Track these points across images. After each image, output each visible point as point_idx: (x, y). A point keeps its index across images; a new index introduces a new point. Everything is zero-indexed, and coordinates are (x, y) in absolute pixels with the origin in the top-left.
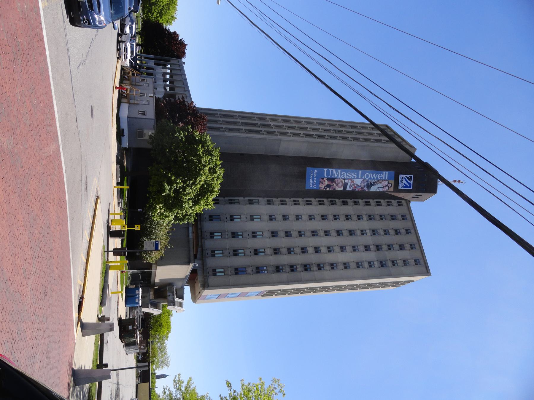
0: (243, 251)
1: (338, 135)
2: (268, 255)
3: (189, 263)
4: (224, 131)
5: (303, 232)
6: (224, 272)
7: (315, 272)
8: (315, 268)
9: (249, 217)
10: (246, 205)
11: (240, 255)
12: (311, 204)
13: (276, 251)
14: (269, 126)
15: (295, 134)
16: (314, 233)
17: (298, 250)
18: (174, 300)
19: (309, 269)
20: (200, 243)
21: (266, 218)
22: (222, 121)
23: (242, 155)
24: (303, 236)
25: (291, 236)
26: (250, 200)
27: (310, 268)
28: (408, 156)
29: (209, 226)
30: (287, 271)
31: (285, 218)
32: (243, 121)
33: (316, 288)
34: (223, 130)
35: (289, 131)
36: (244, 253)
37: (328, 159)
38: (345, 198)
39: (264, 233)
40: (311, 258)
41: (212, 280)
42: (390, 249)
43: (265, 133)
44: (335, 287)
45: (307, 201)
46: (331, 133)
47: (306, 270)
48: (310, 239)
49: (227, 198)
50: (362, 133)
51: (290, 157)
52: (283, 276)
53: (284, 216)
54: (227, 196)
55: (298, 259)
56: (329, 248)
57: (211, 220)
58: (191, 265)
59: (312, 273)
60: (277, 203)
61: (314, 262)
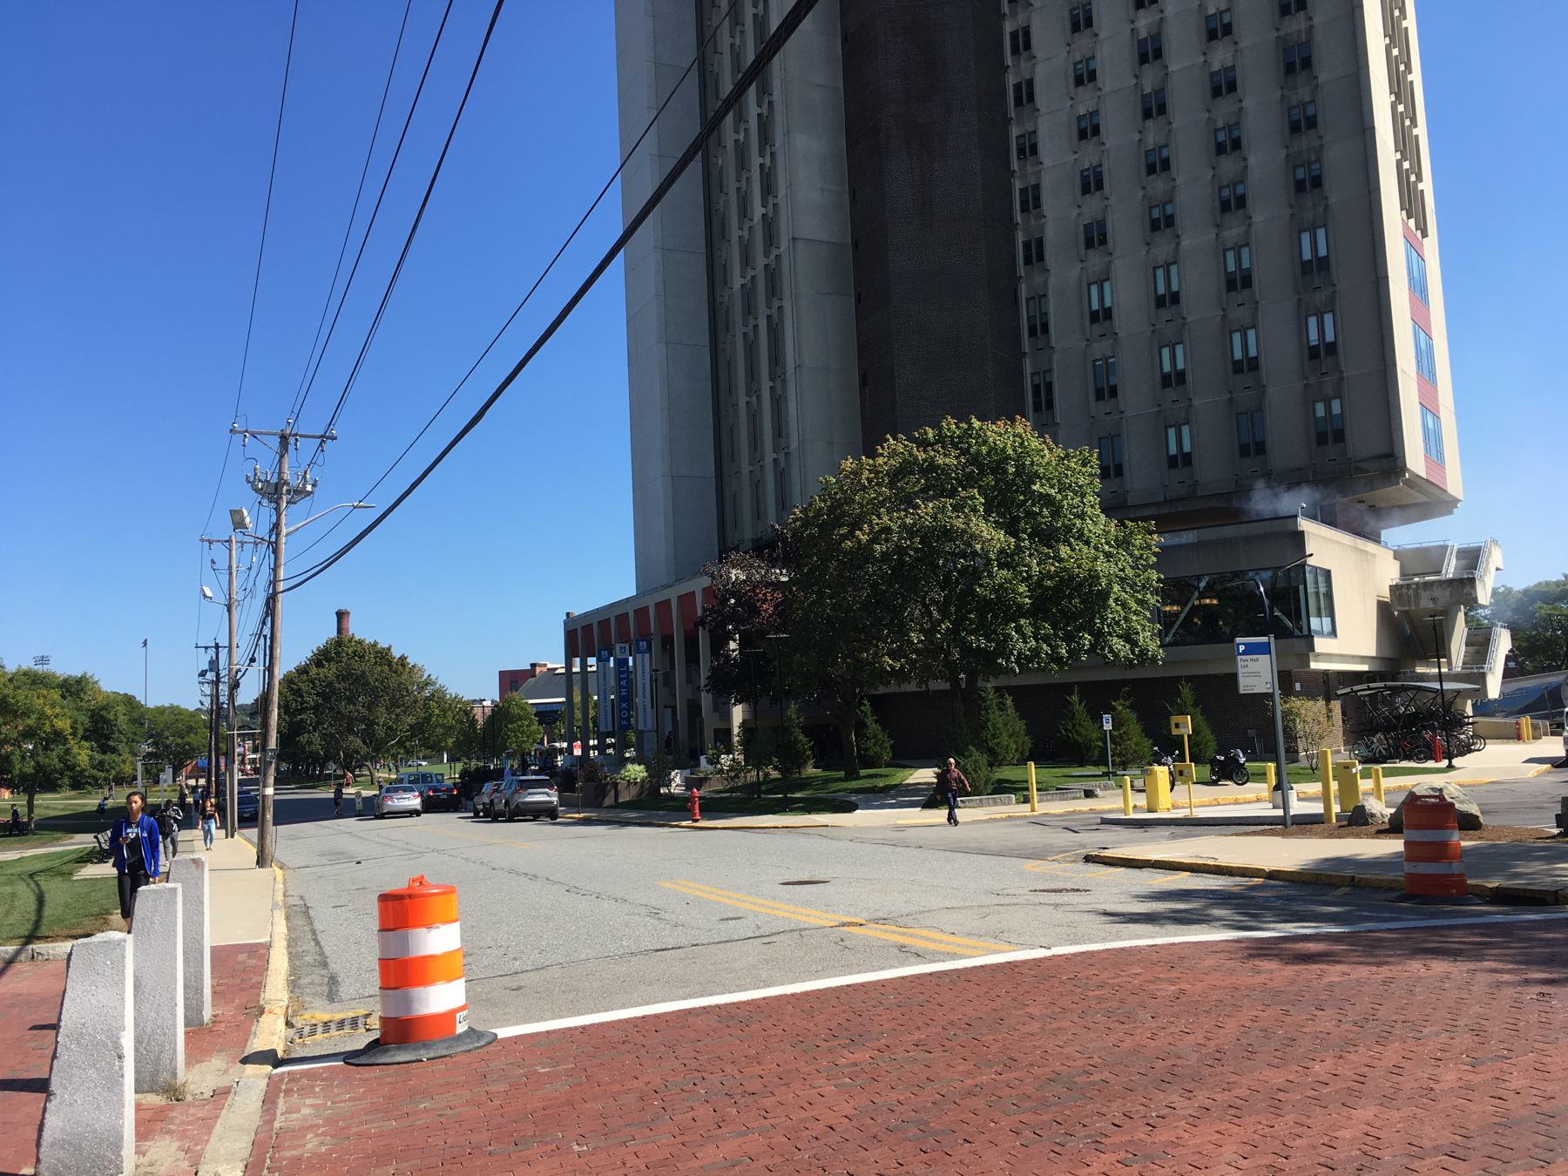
0: (1230, 256)
1: (756, 161)
2: (1247, 233)
3: (1300, 536)
4: (787, 454)
5: (1156, 213)
6: (1313, 231)
7: (1317, 21)
11: (1246, 265)
13: (1232, 203)
14: (748, 293)
15: (768, 189)
18: (1450, 581)
19: (1310, 110)
20: (1212, 504)
21: (1095, 260)
22: (751, 464)
23: (864, 380)
26: (1033, 332)
27: (1305, 104)
29: (1141, 478)
32: (742, 390)
33: (1397, 119)
34: (782, 458)
35: (758, 211)
36: (1237, 249)
37: (845, 39)
39: (1161, 261)
41: (1361, 442)
42: (1228, 29)
44: (1398, 96)
45: (1028, 261)
46: (743, 42)
47: (1307, 63)
51: (853, 194)
52: (1336, 153)
54: (1011, 217)
55: (1259, 107)
56: (1212, 35)
58: (1304, 524)
61: (1284, 153)
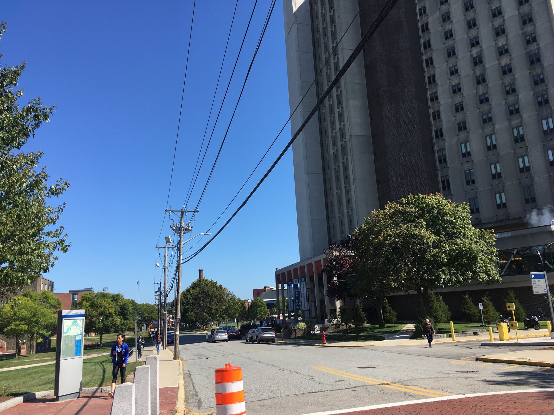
1: (336, 110)
5: (485, 117)
8: (533, 47)
9: (465, 159)
10: (452, 193)
11: (521, 133)
12: (434, 76)
15: (341, 119)
16: (478, 61)
17: (508, 79)
19: (542, 77)
24: (490, 115)
25: (474, 20)
26: (440, 162)
28: (353, 64)
29: (487, 213)
30: (545, 88)
31: (459, 108)
34: (350, 211)
35: (338, 127)
38: (416, 13)
39: (488, 133)
40: (518, 55)
43: (346, 158)
46: (331, 72)
48: (487, 66)
49: (438, 166)
50: (325, 30)
51: (371, 119)
53: (457, 110)
55: (522, 77)
57: (473, 182)
59: (542, 50)
60: (435, 105)
